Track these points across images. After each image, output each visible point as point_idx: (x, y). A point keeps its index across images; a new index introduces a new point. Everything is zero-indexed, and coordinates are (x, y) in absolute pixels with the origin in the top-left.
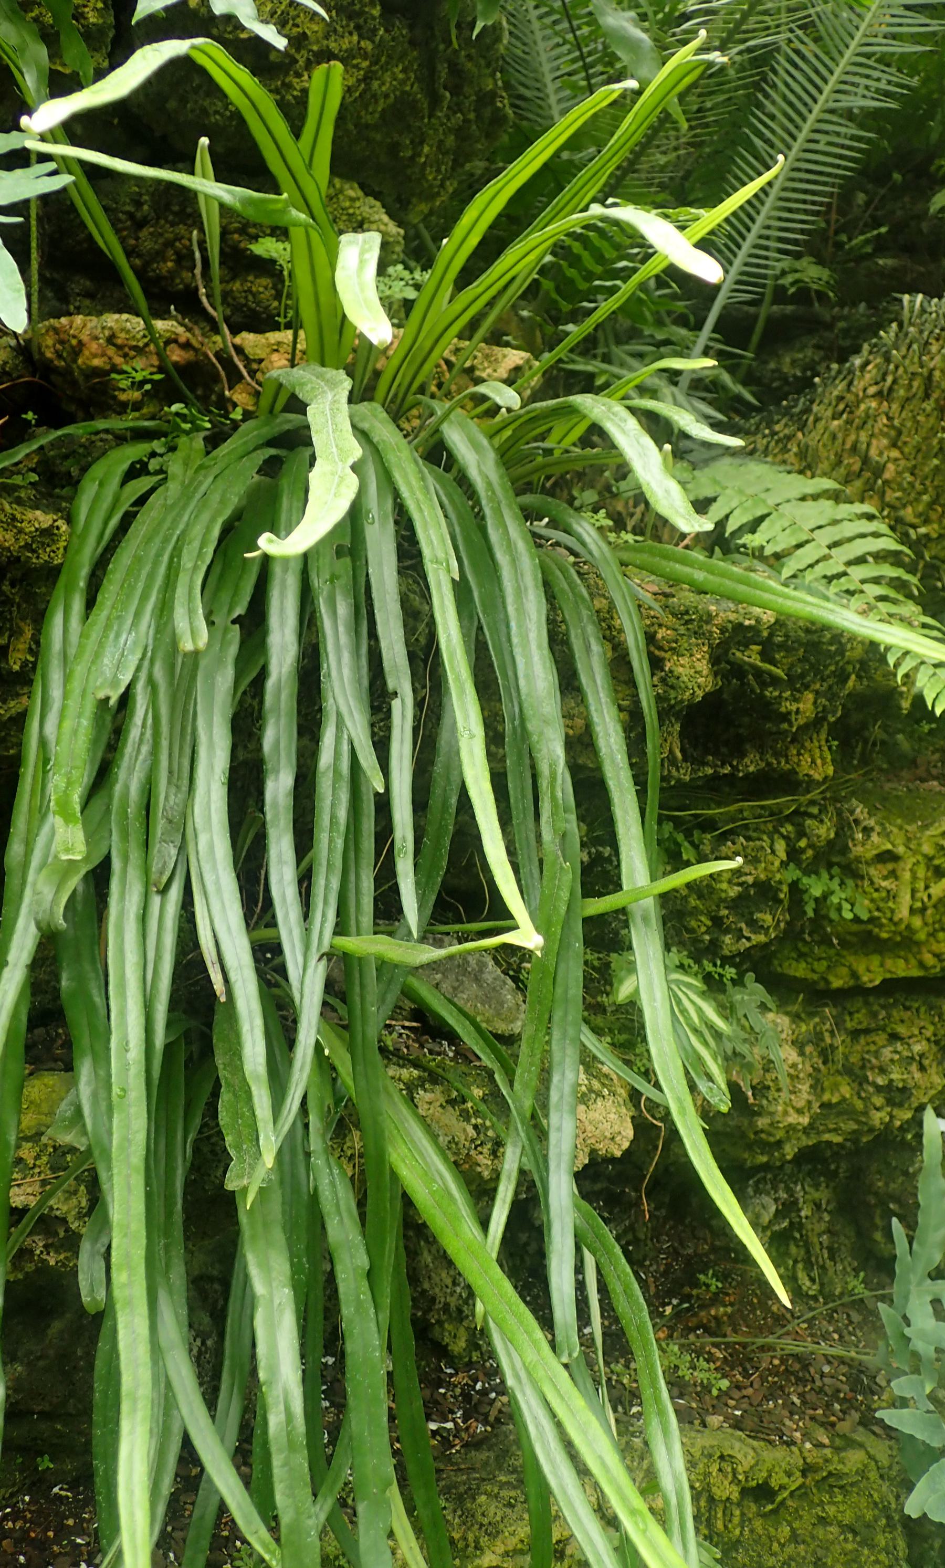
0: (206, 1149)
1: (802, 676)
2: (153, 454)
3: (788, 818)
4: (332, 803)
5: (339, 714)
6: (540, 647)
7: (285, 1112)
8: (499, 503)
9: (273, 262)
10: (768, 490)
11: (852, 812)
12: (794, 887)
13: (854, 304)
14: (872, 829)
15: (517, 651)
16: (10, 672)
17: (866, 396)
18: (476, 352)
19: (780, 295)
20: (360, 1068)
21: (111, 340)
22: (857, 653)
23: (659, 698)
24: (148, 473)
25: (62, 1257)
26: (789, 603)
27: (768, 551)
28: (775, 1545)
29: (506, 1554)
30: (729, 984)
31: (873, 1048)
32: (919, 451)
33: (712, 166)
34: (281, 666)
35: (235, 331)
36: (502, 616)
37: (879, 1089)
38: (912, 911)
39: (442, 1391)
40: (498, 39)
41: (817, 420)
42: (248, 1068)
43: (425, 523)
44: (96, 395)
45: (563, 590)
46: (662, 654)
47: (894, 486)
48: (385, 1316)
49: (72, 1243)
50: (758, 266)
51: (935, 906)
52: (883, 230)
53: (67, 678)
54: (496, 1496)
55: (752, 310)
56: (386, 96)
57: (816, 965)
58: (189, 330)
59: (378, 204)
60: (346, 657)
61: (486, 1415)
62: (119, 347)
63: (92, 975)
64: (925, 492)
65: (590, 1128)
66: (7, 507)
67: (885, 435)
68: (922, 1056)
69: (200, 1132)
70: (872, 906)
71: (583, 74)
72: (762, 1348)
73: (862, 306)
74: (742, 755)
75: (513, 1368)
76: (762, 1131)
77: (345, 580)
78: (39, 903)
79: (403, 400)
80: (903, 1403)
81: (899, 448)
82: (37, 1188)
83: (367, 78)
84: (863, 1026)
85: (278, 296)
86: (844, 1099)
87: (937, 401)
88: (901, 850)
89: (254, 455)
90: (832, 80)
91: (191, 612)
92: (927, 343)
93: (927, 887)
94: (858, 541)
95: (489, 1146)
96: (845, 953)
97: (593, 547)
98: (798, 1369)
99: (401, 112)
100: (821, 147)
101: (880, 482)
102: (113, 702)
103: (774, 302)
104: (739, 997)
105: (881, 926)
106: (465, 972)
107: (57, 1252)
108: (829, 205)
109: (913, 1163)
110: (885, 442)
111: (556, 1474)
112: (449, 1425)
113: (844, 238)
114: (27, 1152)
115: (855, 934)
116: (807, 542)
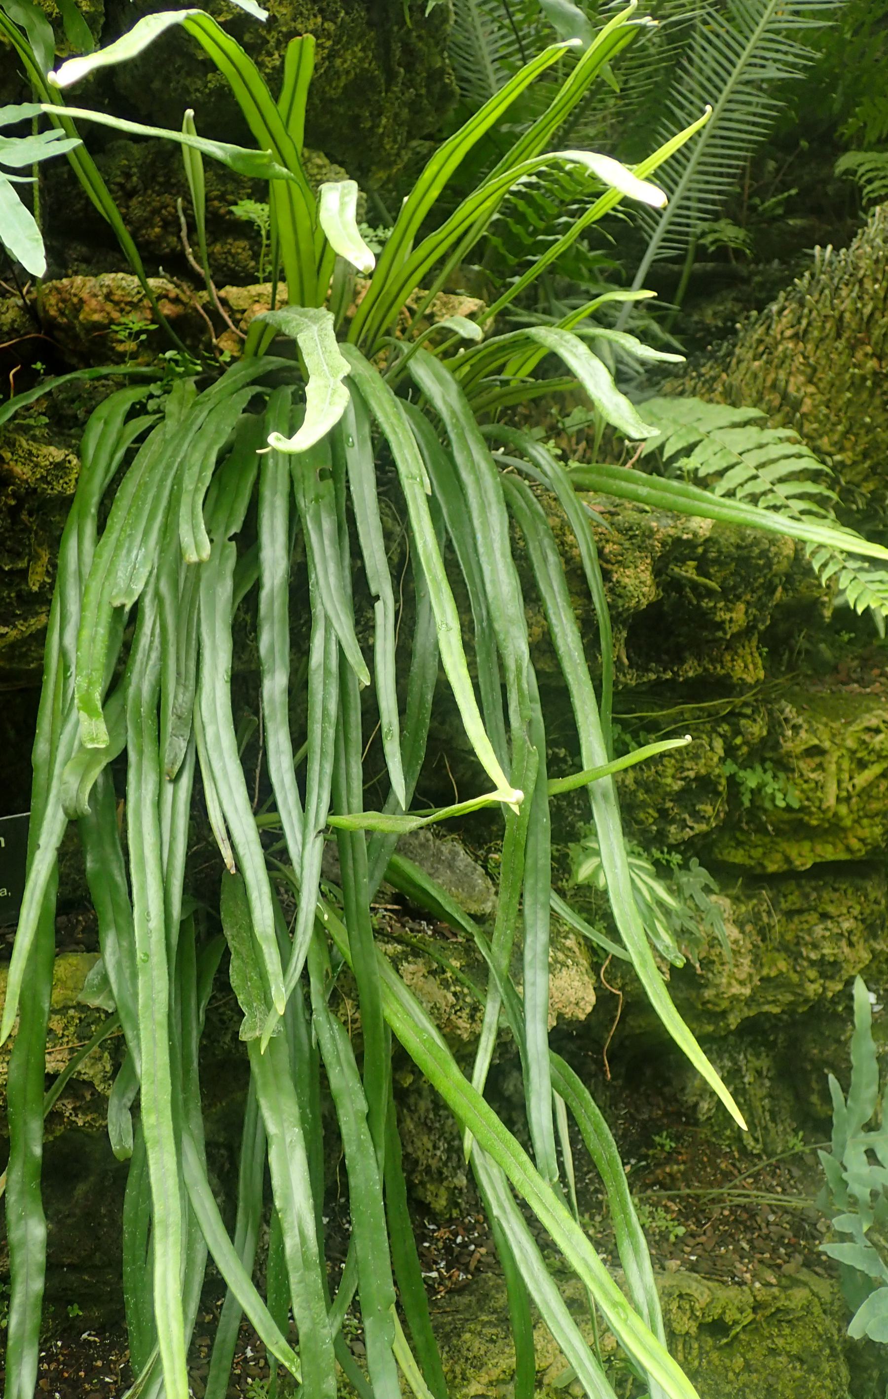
0: (215, 1019)
1: (734, 588)
2: (151, 396)
3: (724, 719)
4: (323, 697)
5: (327, 618)
6: (503, 555)
7: (291, 969)
8: (463, 429)
9: (250, 223)
10: (699, 419)
11: (782, 712)
12: (732, 781)
13: (768, 261)
14: (800, 727)
15: (483, 559)
16: (30, 592)
17: (783, 338)
18: (435, 297)
19: (701, 253)
20: (354, 933)
21: (108, 297)
22: (781, 566)
23: (610, 607)
24: (147, 413)
25: (89, 1118)
26: (725, 511)
27: (702, 473)
28: (731, 1374)
29: (491, 1383)
30: (675, 868)
31: (806, 926)
32: (832, 385)
33: (637, 139)
34: (273, 578)
35: (219, 286)
36: (468, 530)
37: (812, 963)
38: (839, 800)
39: (426, 1244)
40: (445, 20)
41: (739, 362)
42: (258, 929)
43: (400, 444)
44: (97, 346)
45: (521, 508)
46: (609, 567)
47: (811, 418)
48: (381, 1154)
49: (99, 1105)
50: (679, 224)
51: (859, 795)
52: (793, 192)
53: (82, 596)
54: (480, 1333)
55: (676, 267)
56: (348, 72)
57: (753, 853)
58: (177, 286)
59: (343, 170)
60: (332, 567)
61: (467, 1265)
62: (116, 303)
63: (112, 857)
64: (840, 422)
65: (556, 994)
66: (24, 444)
67: (803, 373)
68: (850, 932)
69: (209, 1003)
70: (802, 796)
71: (519, 56)
72: (713, 1201)
73: (776, 263)
74: (682, 661)
75: (498, 1199)
76: (708, 1002)
77: (329, 499)
78: (66, 791)
79: (373, 341)
80: (843, 1237)
81: (815, 384)
82: (66, 1055)
83: (332, 56)
84: (797, 906)
85: (256, 256)
86: (781, 974)
87: (848, 339)
88: (827, 744)
89: (243, 391)
90: (745, 55)
91: (194, 527)
92: (837, 288)
93: (851, 778)
94: (783, 462)
95: (467, 1011)
96: (779, 840)
97: (547, 468)
98: (746, 1218)
99: (361, 87)
100: (735, 116)
101: (798, 415)
102: (127, 609)
103: (697, 259)
104: (685, 879)
105: (811, 814)
106: (439, 861)
107: (84, 1114)
108: (744, 168)
109: (844, 1031)
110: (802, 379)
111: (540, 1291)
112: (434, 1274)
113: (757, 201)
114: (56, 1024)
115: (788, 822)
116: (737, 464)
